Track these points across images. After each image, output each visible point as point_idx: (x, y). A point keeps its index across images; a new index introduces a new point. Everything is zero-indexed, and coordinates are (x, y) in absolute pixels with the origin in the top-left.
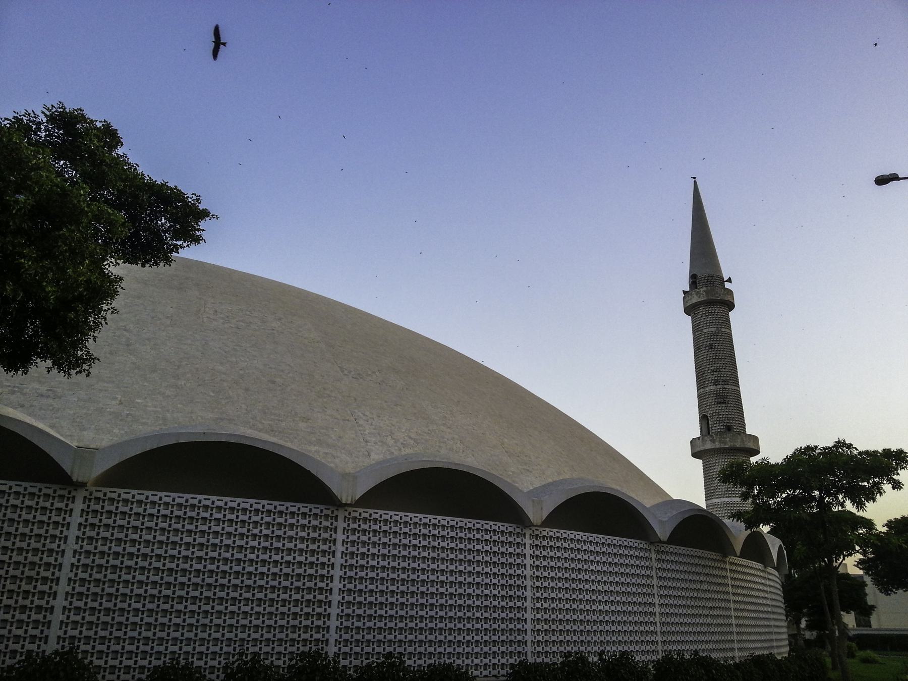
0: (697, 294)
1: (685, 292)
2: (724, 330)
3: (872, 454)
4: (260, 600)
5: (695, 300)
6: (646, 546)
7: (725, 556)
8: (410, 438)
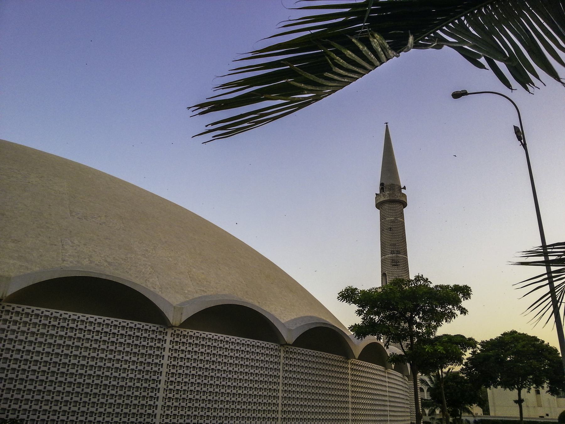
0: (384, 195)
1: (377, 194)
2: (399, 219)
3: (444, 288)
4: (145, 388)
5: (382, 199)
6: (276, 347)
7: (348, 359)
8: (106, 261)
